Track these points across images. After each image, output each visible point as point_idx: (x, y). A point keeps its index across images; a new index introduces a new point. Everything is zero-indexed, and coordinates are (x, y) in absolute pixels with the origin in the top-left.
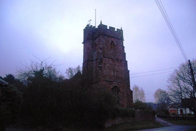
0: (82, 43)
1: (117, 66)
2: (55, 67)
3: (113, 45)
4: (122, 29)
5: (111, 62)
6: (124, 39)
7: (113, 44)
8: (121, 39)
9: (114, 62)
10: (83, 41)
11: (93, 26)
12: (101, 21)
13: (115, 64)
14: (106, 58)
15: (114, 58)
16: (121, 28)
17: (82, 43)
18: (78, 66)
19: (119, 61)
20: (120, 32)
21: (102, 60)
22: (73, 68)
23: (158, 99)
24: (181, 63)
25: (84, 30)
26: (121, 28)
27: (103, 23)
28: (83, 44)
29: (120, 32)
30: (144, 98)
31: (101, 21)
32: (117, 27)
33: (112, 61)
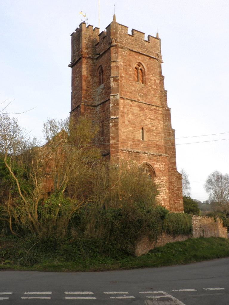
0: (69, 66)
1: (150, 118)
2: (15, 116)
3: (140, 71)
4: (159, 37)
5: (136, 110)
6: (163, 59)
7: (141, 69)
8: (157, 59)
9: (142, 109)
10: (70, 61)
11: (75, 32)
12: (114, 16)
13: (145, 115)
14: (126, 101)
15: (143, 101)
16: (157, 34)
17: (69, 66)
18: (163, 61)
19: (153, 107)
20: (154, 41)
21: (118, 104)
22: (57, 121)
23: (212, 191)
24: (200, 201)
25: (72, 35)
26: (157, 34)
27: (118, 21)
28: (70, 68)
29: (154, 41)
30: (188, 190)
31: (114, 16)
32: (148, 31)
33: (139, 107)
